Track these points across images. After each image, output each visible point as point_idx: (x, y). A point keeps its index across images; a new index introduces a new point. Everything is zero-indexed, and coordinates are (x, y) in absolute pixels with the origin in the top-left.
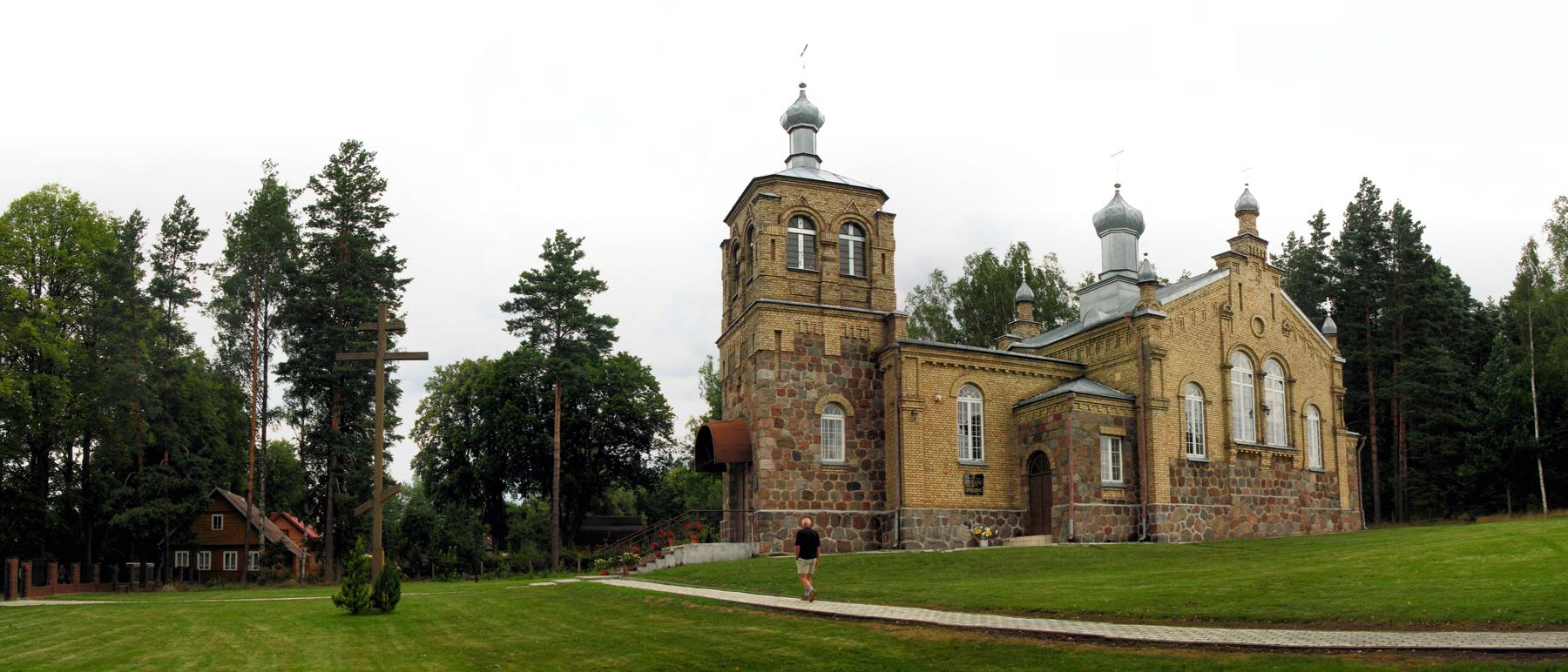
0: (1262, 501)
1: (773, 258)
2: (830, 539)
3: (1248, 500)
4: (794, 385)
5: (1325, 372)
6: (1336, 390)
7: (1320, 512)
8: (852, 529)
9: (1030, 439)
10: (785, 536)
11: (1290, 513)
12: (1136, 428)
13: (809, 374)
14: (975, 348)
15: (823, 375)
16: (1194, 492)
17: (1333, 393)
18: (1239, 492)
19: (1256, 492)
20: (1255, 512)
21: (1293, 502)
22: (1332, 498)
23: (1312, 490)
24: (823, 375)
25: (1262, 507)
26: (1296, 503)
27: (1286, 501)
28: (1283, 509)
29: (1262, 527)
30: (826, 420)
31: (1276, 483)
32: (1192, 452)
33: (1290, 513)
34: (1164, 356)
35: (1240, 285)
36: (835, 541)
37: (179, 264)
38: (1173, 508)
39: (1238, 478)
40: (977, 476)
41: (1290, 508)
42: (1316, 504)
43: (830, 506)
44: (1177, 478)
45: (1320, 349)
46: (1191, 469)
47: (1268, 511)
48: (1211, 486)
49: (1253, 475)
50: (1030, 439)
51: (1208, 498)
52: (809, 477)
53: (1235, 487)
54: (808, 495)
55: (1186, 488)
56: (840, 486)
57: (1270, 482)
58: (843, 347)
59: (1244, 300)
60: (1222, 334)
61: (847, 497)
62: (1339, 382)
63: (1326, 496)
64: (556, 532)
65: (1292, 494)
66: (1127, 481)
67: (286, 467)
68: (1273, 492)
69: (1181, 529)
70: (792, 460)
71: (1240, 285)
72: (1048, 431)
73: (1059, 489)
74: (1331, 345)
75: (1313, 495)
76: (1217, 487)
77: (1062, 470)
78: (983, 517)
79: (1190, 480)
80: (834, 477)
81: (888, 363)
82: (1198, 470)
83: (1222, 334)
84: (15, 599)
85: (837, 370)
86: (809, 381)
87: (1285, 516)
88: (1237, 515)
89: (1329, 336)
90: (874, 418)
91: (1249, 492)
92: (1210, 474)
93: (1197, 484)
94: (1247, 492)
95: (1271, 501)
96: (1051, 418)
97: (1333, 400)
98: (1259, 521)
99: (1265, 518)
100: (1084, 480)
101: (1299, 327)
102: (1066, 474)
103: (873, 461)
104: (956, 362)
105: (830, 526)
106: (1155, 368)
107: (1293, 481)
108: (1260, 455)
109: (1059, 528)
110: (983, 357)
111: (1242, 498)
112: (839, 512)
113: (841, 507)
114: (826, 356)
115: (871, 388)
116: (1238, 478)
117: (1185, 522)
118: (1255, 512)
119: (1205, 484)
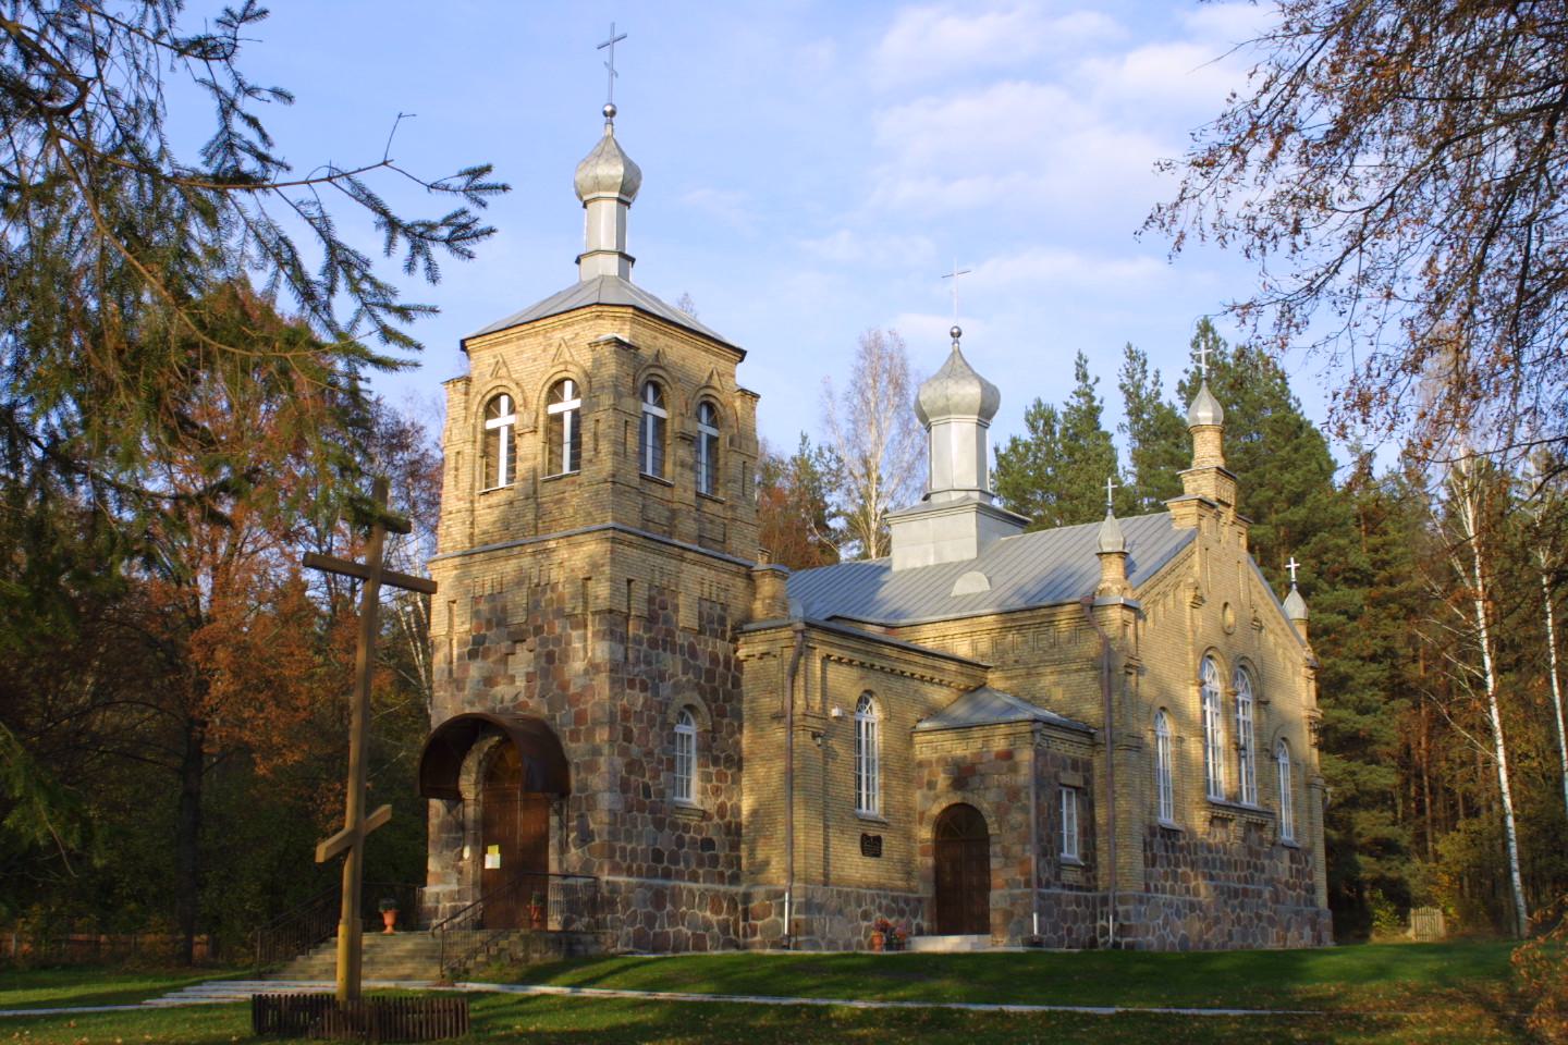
0: (1236, 894)
1: (626, 456)
4: (646, 672)
23: (1285, 877)
25: (1236, 902)
30: (682, 735)
36: (690, 933)
37: (1322, 516)
38: (1149, 899)
41: (1265, 905)
61: (701, 864)
67: (619, 807)
69: (1158, 933)
70: (641, 797)
78: (884, 902)
79: (1161, 856)
82: (1169, 843)
84: (1029, 1013)
87: (1259, 917)
107: (1266, 862)
115: (730, 686)
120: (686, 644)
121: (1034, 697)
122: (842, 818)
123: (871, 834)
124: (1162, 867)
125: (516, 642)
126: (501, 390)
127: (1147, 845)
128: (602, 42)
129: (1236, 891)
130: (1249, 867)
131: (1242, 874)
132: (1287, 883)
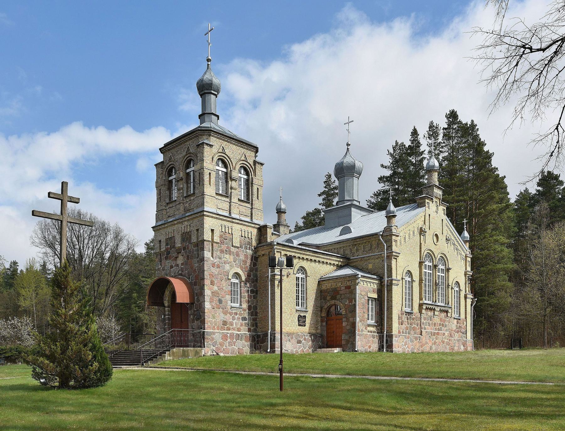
2: (235, 347)
5: (463, 262)
6: (468, 273)
8: (244, 342)
9: (328, 298)
10: (216, 345)
11: (446, 340)
12: (381, 294)
13: (226, 256)
14: (327, 253)
15: (232, 257)
16: (407, 328)
17: (465, 275)
19: (432, 329)
23: (454, 328)
24: (232, 257)
25: (434, 337)
26: (448, 335)
29: (434, 347)
32: (298, 306)
33: (446, 340)
34: (398, 256)
35: (429, 215)
39: (425, 322)
40: (304, 316)
41: (445, 338)
42: (457, 336)
43: (234, 329)
44: (400, 321)
45: (461, 250)
47: (437, 339)
50: (328, 298)
51: (412, 332)
52: (225, 313)
54: (225, 323)
55: (404, 326)
56: (238, 319)
58: (240, 242)
60: (421, 244)
62: (469, 269)
66: (376, 322)
68: (439, 330)
70: (218, 304)
71: (429, 215)
72: (341, 295)
73: (348, 325)
74: (467, 246)
77: (350, 315)
80: (236, 314)
81: (263, 253)
82: (409, 317)
83: (421, 244)
85: (238, 255)
86: (226, 260)
87: (443, 342)
89: (465, 242)
90: (253, 282)
92: (413, 319)
95: (438, 334)
96: (343, 288)
97: (466, 279)
101: (453, 238)
102: (352, 317)
103: (252, 306)
105: (235, 340)
106: (394, 262)
107: (447, 323)
108: (434, 309)
109: (347, 344)
110: (308, 253)
112: (239, 333)
113: (239, 330)
114: (233, 246)
116: (425, 322)
120: (235, 252)
121: (363, 268)
122: (26, 325)
123: (302, 315)
124: (406, 325)
125: (178, 253)
126: (172, 166)
127: (298, 318)
128: (206, 33)
129: (434, 333)
130: (440, 325)
131: (437, 327)
132: (454, 331)
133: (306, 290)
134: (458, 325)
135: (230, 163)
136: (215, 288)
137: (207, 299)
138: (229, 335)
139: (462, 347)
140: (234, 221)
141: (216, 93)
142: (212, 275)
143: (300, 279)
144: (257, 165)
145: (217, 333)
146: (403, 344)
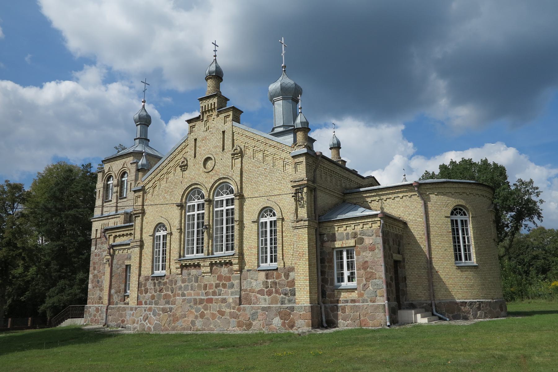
0: (201, 302)
3: (189, 301)
7: (264, 309)
11: (228, 310)
16: (153, 297)
18: (183, 295)
20: (194, 311)
21: (231, 301)
22: (286, 294)
23: (261, 287)
27: (224, 301)
28: (220, 307)
31: (217, 286)
39: (183, 285)
46: (152, 282)
48: (165, 292)
49: (197, 281)
51: (162, 301)
53: (180, 292)
57: (212, 285)
59: (197, 149)
63: (277, 292)
64: (184, 298)
65: (232, 294)
68: (214, 293)
75: (261, 292)
76: (170, 293)
87: (222, 313)
88: (178, 314)
91: (192, 295)
92: (165, 284)
93: (155, 292)
94: (190, 294)
98: (196, 317)
99: (202, 315)
100: (116, 293)
104: (125, 233)
111: (184, 300)
116: (183, 285)
117: (142, 318)
118: (194, 311)
119: (161, 291)
133: (258, 254)
134: (269, 281)
135: (120, 171)
136: (96, 272)
137: (90, 281)
138: (100, 308)
139: (277, 322)
140: (109, 217)
141: (148, 124)
142: (94, 263)
143: (224, 248)
144: (135, 165)
145: (93, 306)
146: (141, 319)
